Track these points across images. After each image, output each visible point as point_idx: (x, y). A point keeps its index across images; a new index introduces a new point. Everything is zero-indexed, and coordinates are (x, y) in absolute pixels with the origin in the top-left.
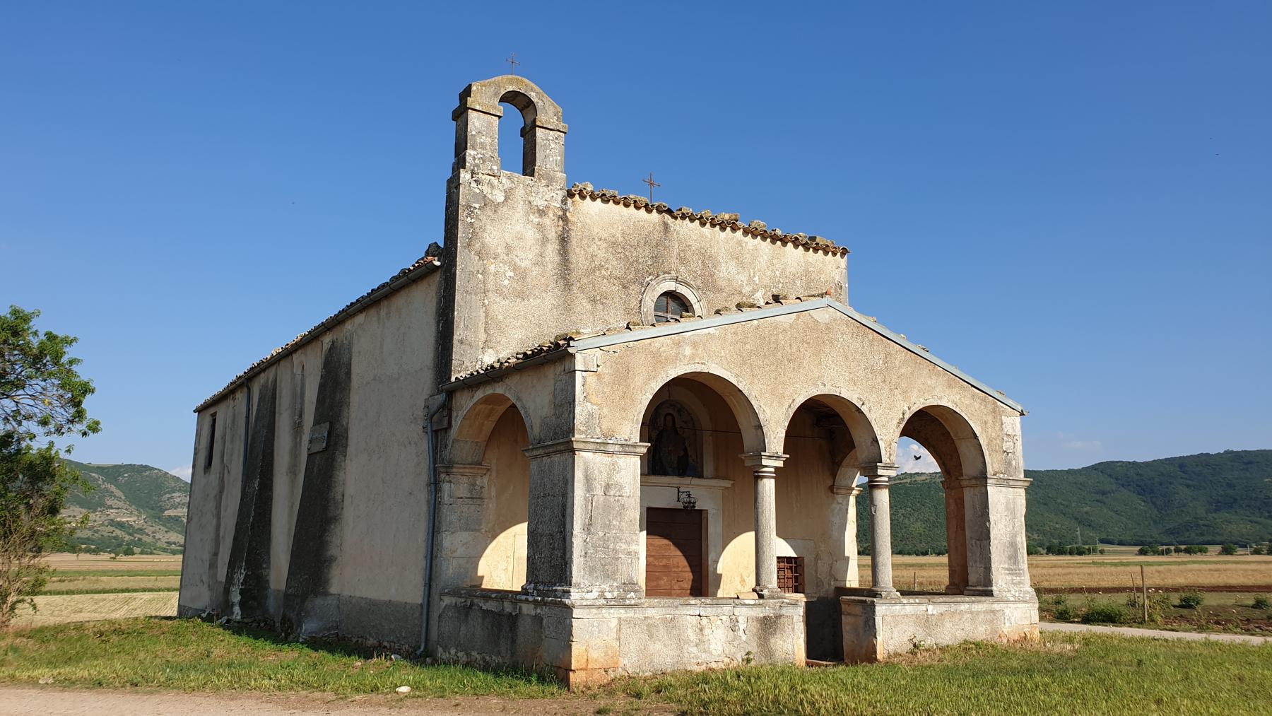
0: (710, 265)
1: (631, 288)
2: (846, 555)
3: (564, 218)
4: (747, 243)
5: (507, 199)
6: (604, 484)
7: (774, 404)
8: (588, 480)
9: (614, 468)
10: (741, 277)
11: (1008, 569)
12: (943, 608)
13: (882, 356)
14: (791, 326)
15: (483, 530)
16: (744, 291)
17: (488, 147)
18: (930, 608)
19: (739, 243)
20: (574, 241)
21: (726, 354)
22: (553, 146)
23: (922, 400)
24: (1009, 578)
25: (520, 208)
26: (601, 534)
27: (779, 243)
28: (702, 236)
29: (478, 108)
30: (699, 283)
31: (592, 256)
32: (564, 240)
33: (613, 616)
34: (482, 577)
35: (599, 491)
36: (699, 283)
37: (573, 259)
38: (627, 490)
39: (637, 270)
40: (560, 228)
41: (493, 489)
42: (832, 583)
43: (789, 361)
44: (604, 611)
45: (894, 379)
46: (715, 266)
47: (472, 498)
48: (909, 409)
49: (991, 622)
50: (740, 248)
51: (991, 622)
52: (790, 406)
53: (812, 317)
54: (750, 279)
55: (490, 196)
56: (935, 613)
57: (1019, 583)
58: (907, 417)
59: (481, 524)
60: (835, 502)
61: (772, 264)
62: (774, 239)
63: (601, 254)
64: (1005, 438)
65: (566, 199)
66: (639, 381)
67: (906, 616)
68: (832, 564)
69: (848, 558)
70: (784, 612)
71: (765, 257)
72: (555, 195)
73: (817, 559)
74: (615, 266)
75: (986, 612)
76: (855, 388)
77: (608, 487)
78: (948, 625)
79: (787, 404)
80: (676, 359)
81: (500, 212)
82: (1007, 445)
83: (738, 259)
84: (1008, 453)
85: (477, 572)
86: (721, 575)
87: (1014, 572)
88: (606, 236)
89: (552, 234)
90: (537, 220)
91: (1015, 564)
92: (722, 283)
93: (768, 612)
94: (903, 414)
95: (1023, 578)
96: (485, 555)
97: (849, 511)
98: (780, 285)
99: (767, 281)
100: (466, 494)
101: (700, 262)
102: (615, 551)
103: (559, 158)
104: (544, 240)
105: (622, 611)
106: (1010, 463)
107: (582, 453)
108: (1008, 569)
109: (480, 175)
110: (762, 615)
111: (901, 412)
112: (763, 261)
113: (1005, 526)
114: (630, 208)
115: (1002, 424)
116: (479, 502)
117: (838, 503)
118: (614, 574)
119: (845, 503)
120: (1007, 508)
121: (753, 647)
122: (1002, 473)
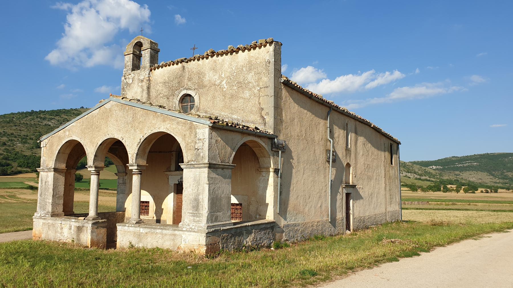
0: (201, 77)
1: (170, 98)
2: (266, 202)
3: (149, 80)
4: (218, 60)
5: (132, 82)
6: (45, 181)
7: (91, 147)
8: (42, 180)
9: (47, 176)
10: (215, 77)
11: (192, 213)
12: (147, 230)
13: (132, 115)
14: (98, 114)
15: (126, 194)
16: (216, 83)
17: (129, 66)
18: (141, 229)
19: (215, 62)
20: (152, 87)
21: (77, 131)
22: (147, 55)
23: (149, 131)
24: (192, 218)
25: (136, 82)
26: (43, 197)
27: (234, 53)
28: (199, 65)
29: (126, 54)
30: (196, 87)
31: (157, 90)
32: (149, 88)
33: (42, 221)
34: (126, 208)
35: (44, 184)
36: (196, 87)
37: (151, 94)
38: (50, 183)
39: (172, 90)
40: (148, 84)
41: (128, 180)
42: (258, 217)
43: (97, 128)
44: (39, 220)
45: (137, 124)
46: (203, 77)
47: (123, 183)
48: (143, 137)
49: (173, 240)
50: (215, 64)
51: (173, 240)
52: (96, 146)
53: (105, 108)
54: (220, 76)
55: (128, 82)
56: (143, 232)
57: (198, 221)
58: (142, 141)
59: (125, 192)
60: (261, 176)
61: (231, 65)
62: (232, 52)
63: (160, 88)
64: (197, 142)
65: (150, 73)
66: (55, 147)
67: (129, 232)
68: (258, 207)
69: (268, 204)
70: (85, 225)
71: (228, 63)
72: (146, 73)
73: (249, 204)
74: (165, 91)
75: (171, 235)
76: (120, 133)
77: (46, 182)
78: (149, 239)
79: (95, 145)
80: (63, 138)
81: (131, 86)
82: (199, 145)
83: (214, 69)
84: (198, 150)
85: (124, 207)
86: (163, 209)
87: (195, 215)
88: (162, 81)
89: (145, 88)
90: (141, 84)
91: (197, 210)
92: (206, 83)
93: (80, 225)
94: (140, 140)
95: (201, 218)
96: (126, 201)
97: (269, 180)
98: (235, 74)
99: (228, 74)
100: (122, 182)
101: (197, 77)
102: (46, 202)
103: (148, 59)
104: (143, 90)
105: (43, 220)
106: (199, 155)
107: (41, 172)
108: (192, 213)
109: (126, 76)
110: (78, 226)
111: (139, 139)
112: (226, 66)
113: (192, 190)
114: (214, 57)
115: (196, 134)
116: (125, 184)
117: (263, 176)
118: (45, 209)
119: (267, 176)
120: (195, 180)
121: (75, 237)
122: (193, 161)
